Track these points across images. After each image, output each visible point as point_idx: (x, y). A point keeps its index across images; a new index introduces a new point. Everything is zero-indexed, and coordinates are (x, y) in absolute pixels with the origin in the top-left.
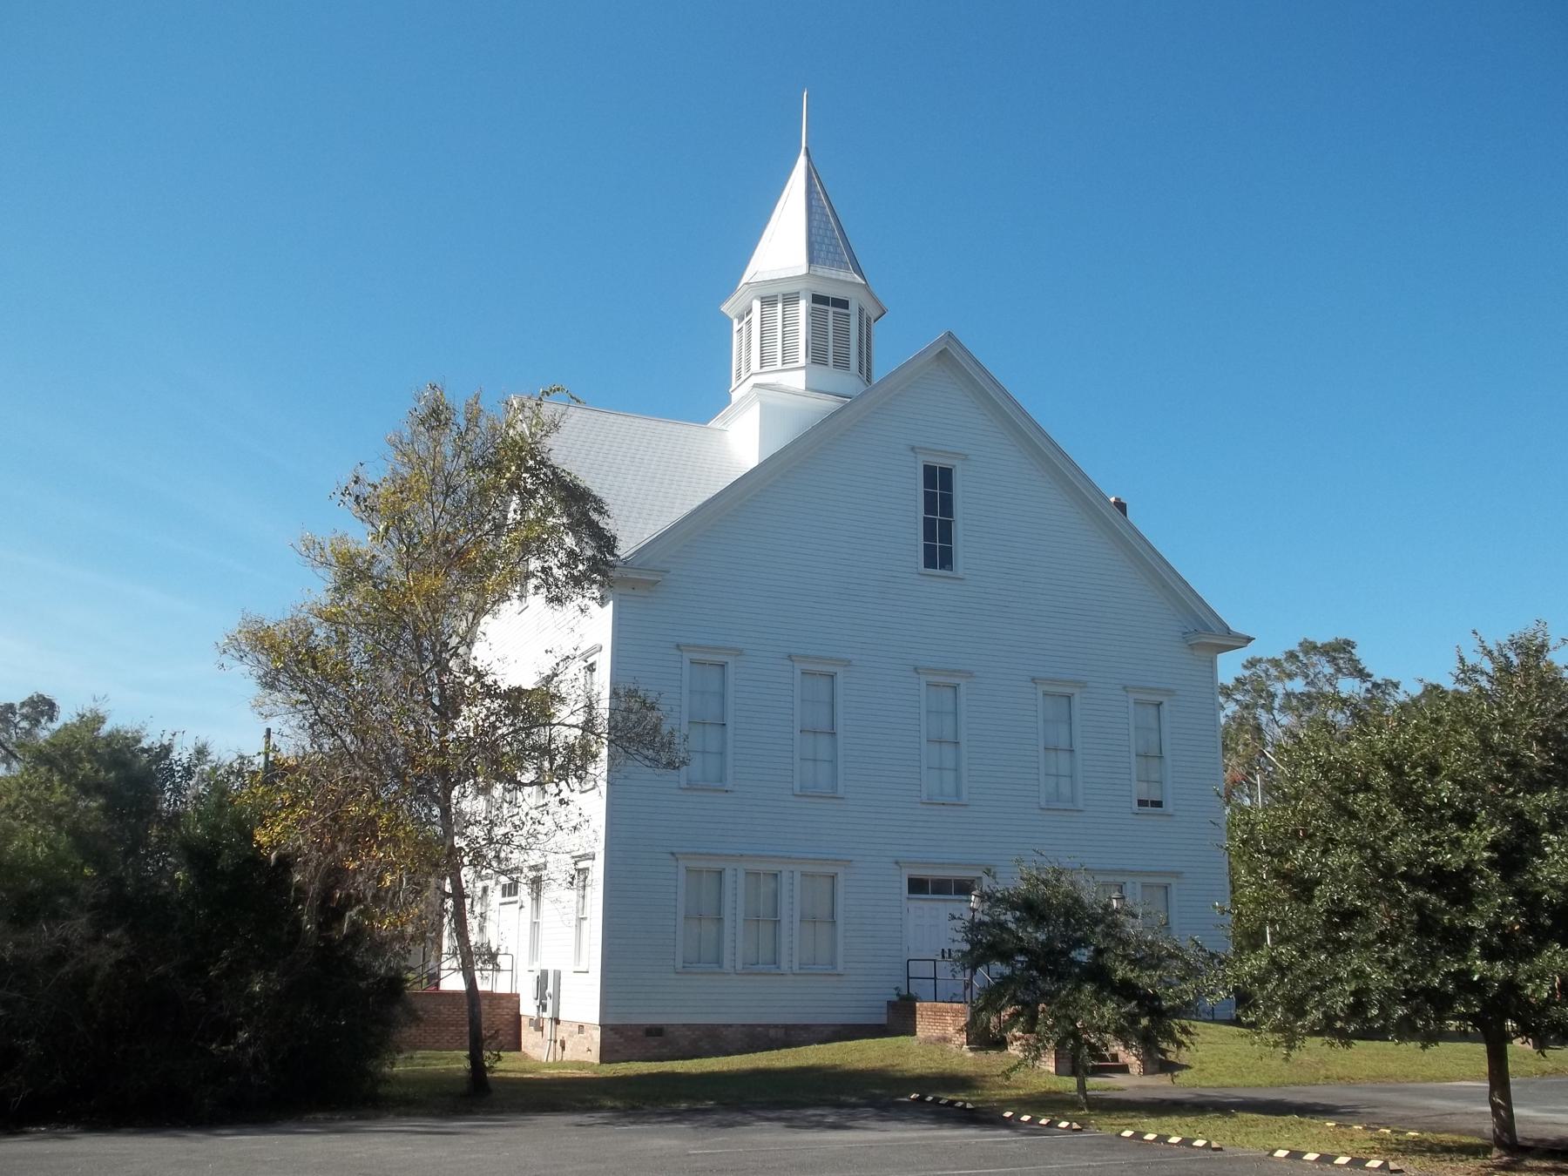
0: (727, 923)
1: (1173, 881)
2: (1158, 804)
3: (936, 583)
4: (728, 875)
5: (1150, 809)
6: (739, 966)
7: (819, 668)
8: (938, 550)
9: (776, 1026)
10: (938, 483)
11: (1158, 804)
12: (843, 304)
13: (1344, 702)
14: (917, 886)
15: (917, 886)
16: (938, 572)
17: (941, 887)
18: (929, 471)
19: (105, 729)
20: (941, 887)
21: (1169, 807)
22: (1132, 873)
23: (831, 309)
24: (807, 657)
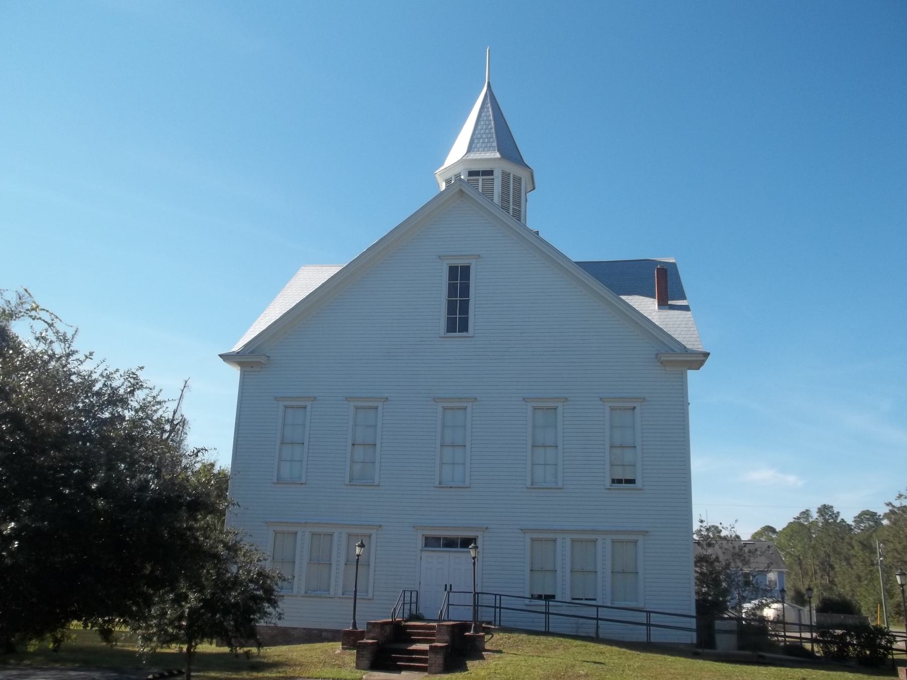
0: (334, 567)
1: (640, 538)
2: (632, 481)
3: (457, 341)
4: (336, 536)
5: (624, 485)
6: (303, 592)
7: (371, 404)
8: (458, 318)
9: (326, 630)
10: (459, 279)
11: (632, 481)
12: (490, 173)
13: (132, 392)
14: (431, 542)
15: (431, 542)
16: (457, 334)
17: (450, 543)
18: (453, 270)
19: (216, 470)
20: (450, 543)
21: (639, 484)
22: (564, 531)
23: (480, 178)
24: (465, 398)
